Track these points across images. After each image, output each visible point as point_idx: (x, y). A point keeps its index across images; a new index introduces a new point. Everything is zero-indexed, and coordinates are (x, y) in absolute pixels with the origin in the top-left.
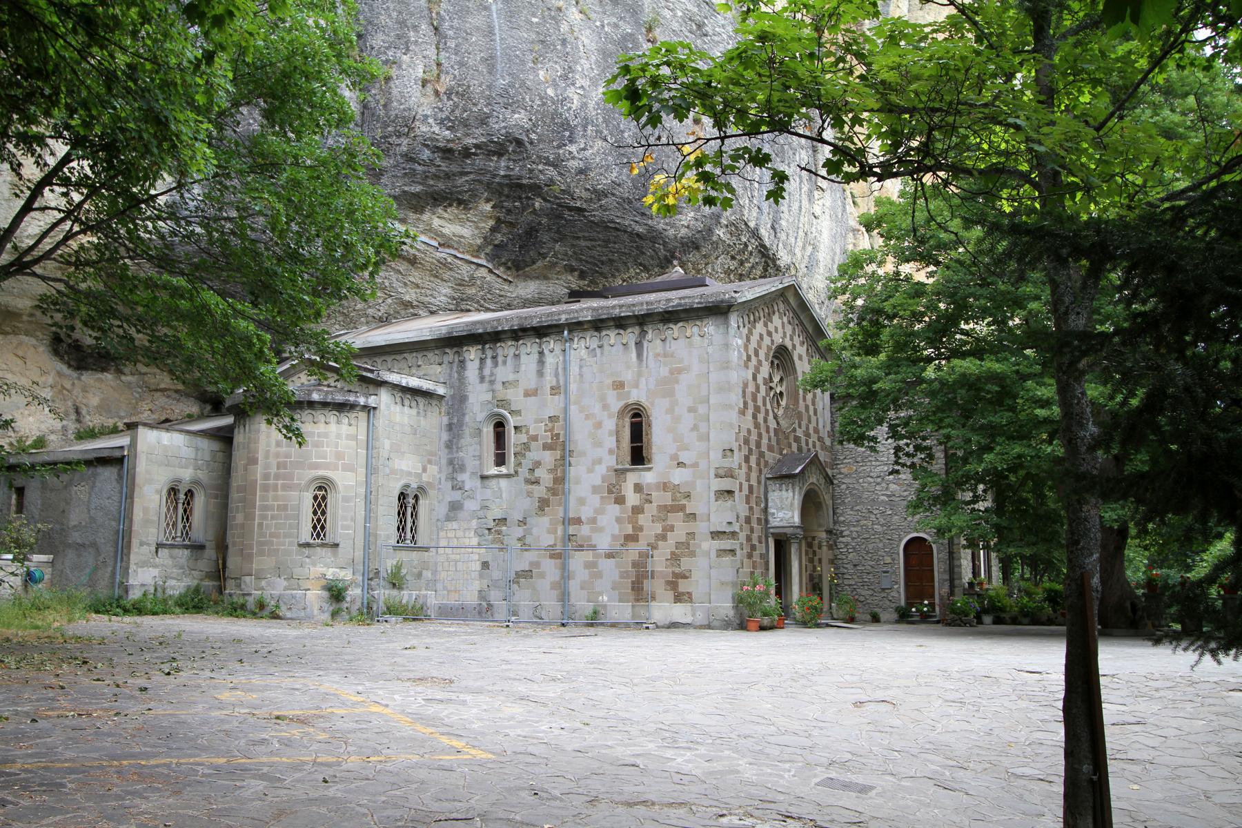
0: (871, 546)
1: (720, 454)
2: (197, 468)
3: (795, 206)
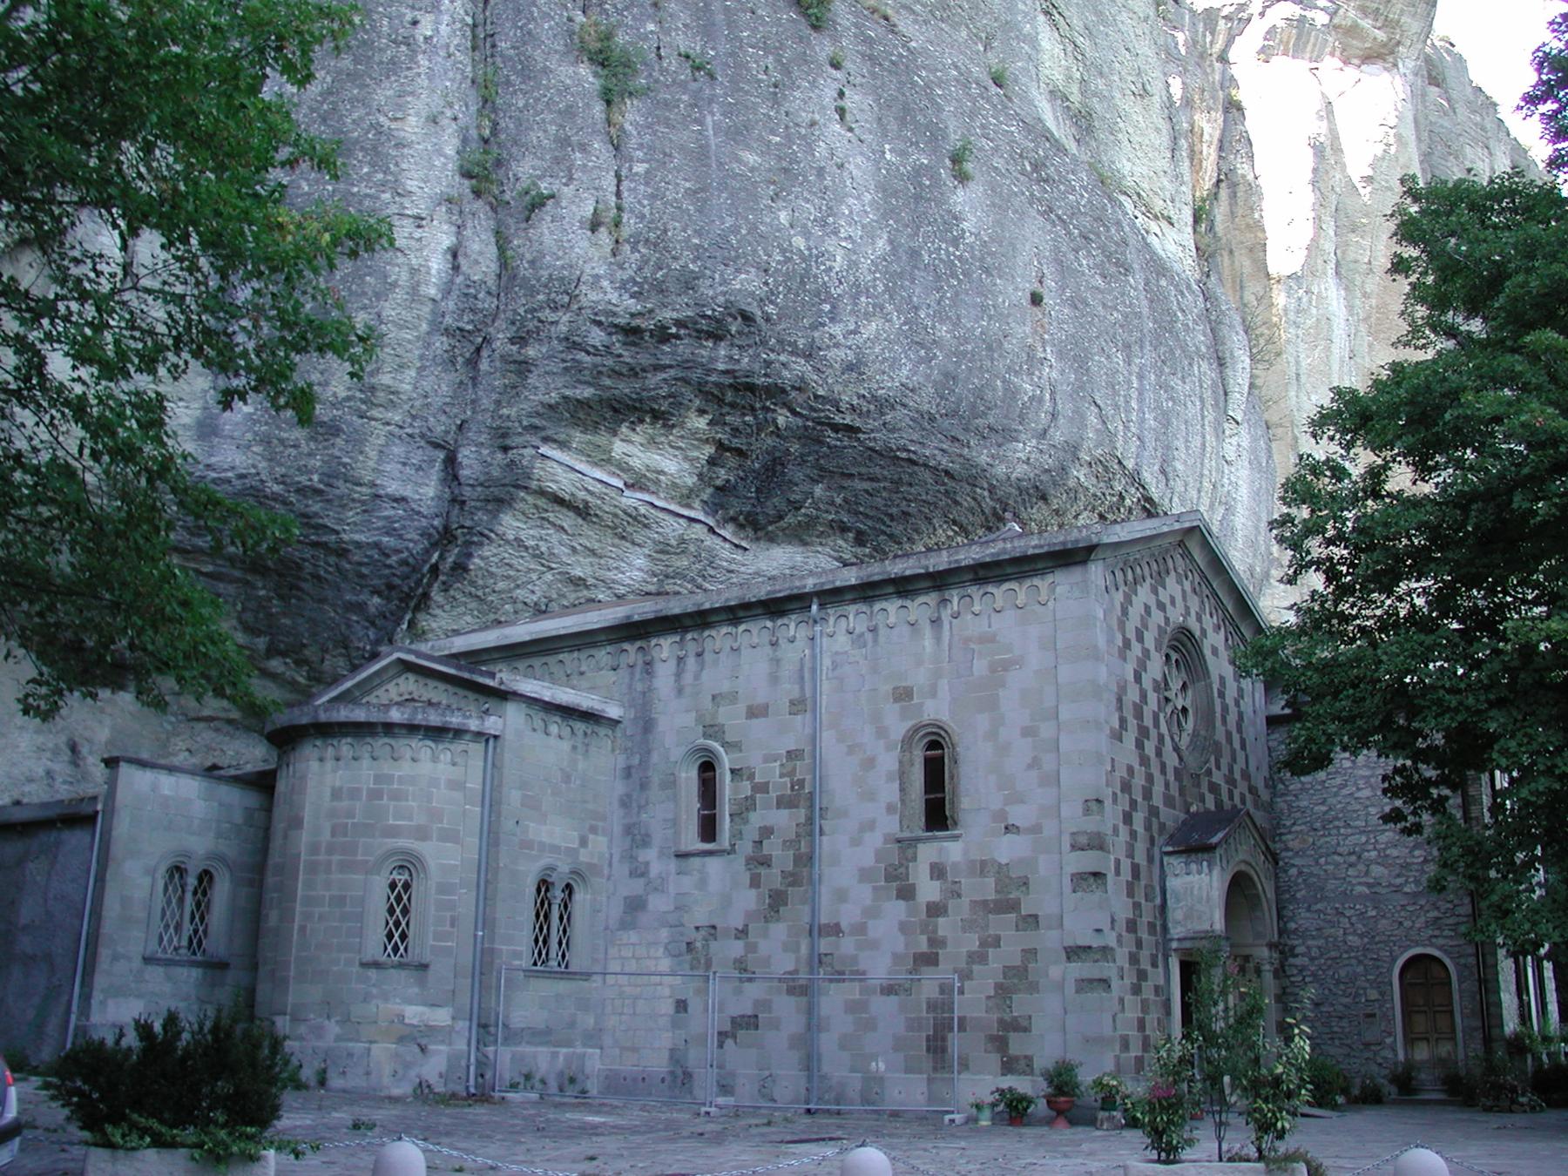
0: (1343, 973)
1: (1080, 811)
2: (219, 835)
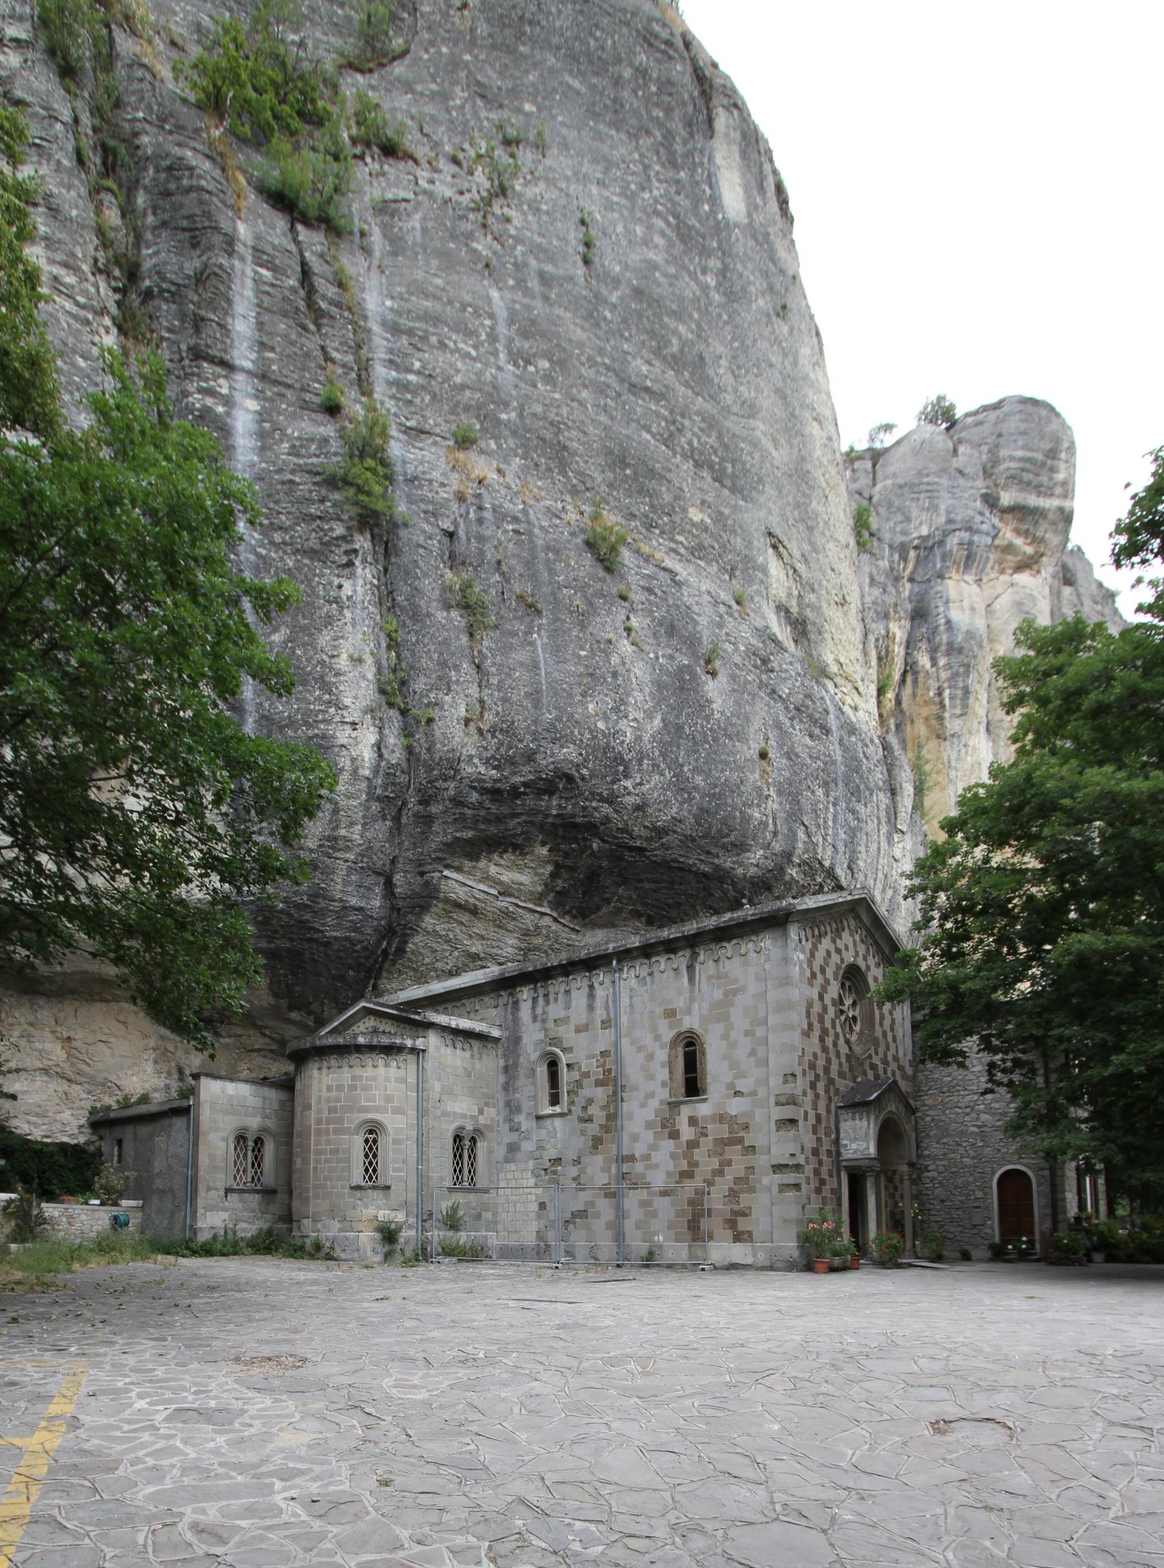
0: (959, 1181)
1: (781, 1080)
2: (264, 1117)
3: (873, 847)
